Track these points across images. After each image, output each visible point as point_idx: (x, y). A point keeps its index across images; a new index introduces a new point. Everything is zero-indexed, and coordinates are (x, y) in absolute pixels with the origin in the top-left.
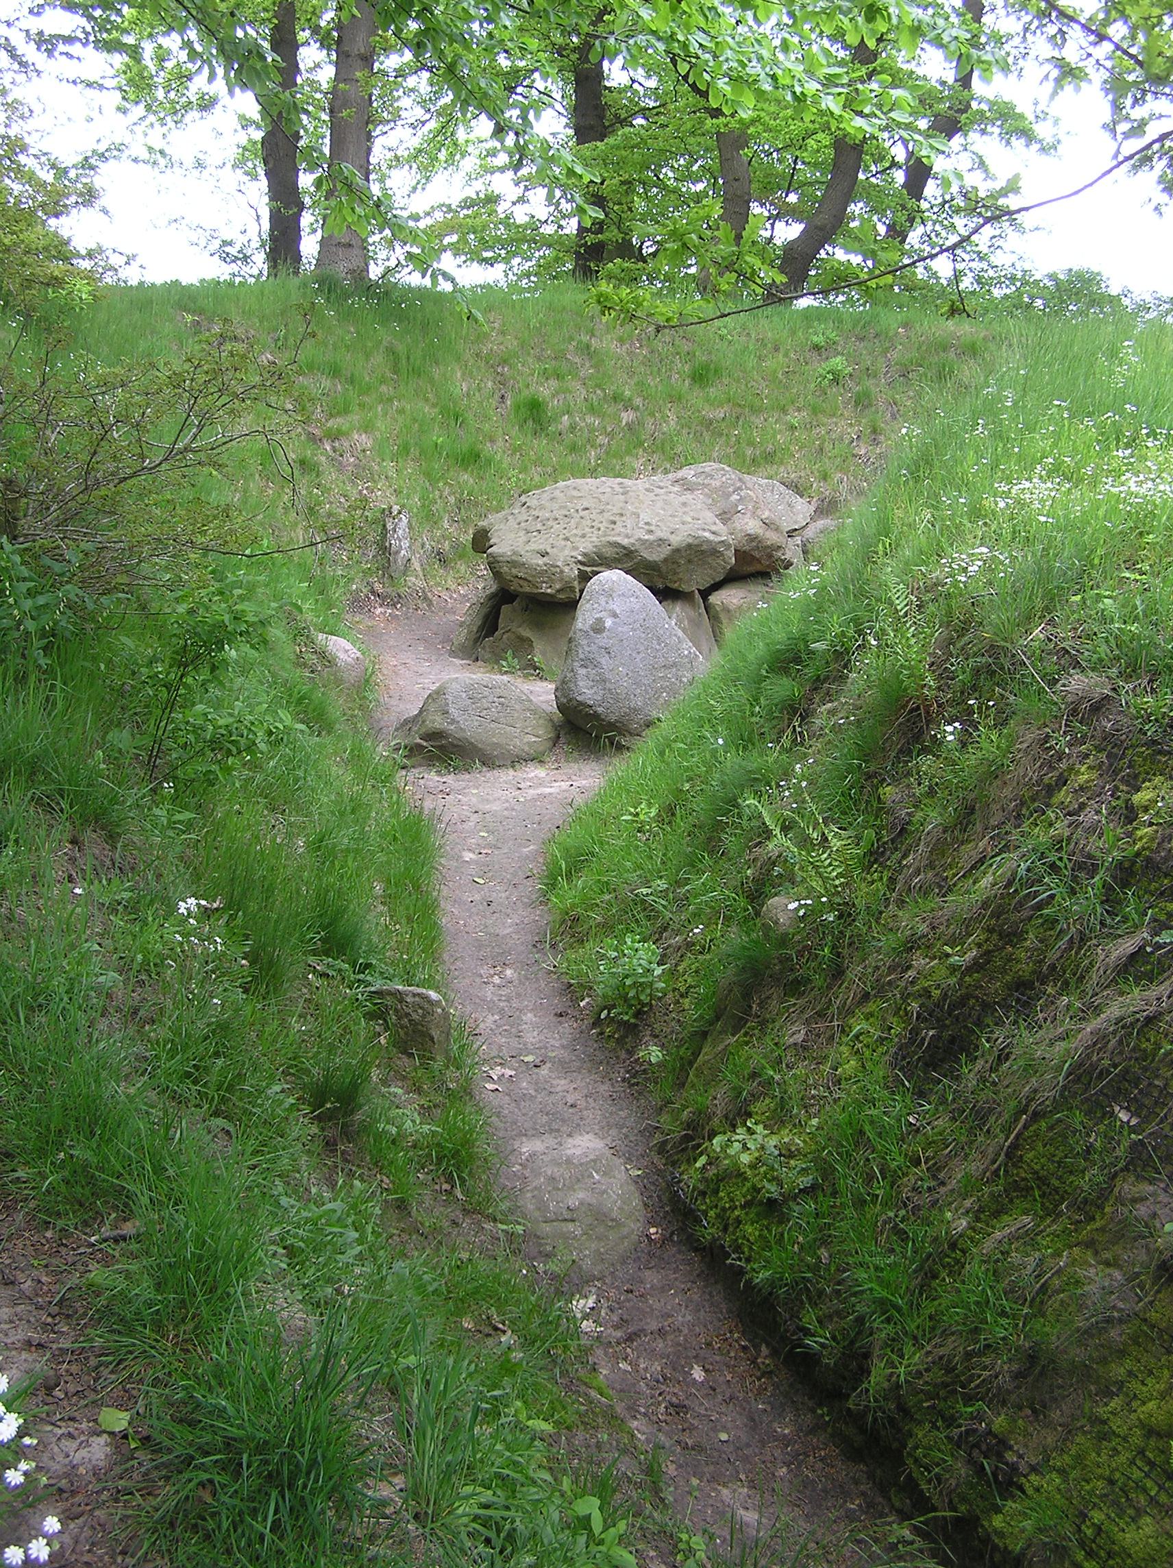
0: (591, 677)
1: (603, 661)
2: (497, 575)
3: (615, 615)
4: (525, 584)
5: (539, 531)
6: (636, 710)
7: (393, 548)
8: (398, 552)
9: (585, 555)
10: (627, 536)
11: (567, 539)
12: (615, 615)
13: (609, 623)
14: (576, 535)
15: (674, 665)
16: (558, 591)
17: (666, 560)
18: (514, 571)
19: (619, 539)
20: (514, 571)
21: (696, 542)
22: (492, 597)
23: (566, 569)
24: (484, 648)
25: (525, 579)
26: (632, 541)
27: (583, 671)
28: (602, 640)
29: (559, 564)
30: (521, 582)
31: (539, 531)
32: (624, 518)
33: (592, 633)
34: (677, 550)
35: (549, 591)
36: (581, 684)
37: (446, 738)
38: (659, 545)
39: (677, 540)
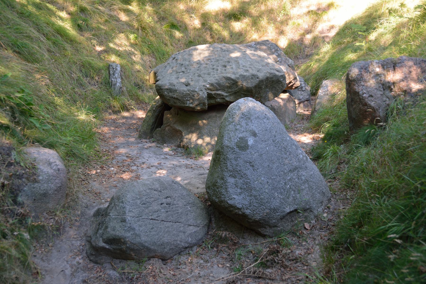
0: (240, 185)
1: (248, 173)
2: (162, 96)
3: (254, 135)
4: (178, 102)
5: (183, 72)
6: (275, 210)
7: (113, 83)
8: (115, 84)
9: (212, 85)
10: (234, 73)
11: (199, 76)
12: (254, 135)
13: (251, 141)
14: (204, 74)
15: (296, 168)
16: (197, 106)
17: (255, 87)
18: (170, 94)
19: (229, 75)
20: (170, 94)
21: (271, 76)
22: (160, 106)
23: (201, 93)
24: (156, 134)
25: (177, 99)
26: (237, 76)
27: (231, 180)
28: (244, 156)
29: (197, 90)
30: (175, 101)
31: (183, 72)
32: (230, 64)
33: (237, 150)
34: (261, 81)
35: (191, 105)
36: (230, 190)
37: (125, 243)
38: (252, 78)
39: (261, 75)
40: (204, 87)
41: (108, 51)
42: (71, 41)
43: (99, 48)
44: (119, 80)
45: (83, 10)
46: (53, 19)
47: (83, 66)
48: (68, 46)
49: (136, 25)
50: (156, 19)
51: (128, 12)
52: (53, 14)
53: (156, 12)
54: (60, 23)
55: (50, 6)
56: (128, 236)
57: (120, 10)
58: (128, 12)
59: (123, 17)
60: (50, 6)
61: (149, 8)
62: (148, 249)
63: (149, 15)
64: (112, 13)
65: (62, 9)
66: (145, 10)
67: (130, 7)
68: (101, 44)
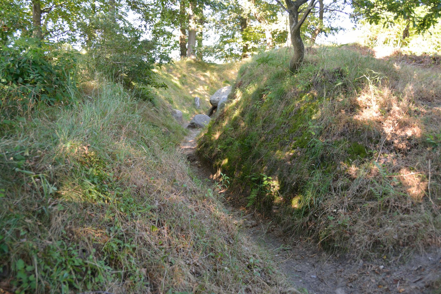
40: (429, 236)
41: (194, 93)
42: (180, 89)
43: (191, 92)
44: (199, 103)
45: (184, 76)
46: (173, 80)
47: (185, 98)
48: (178, 90)
49: (208, 82)
50: (219, 79)
51: (205, 76)
52: (172, 78)
53: (219, 76)
54: (175, 82)
55: (171, 75)
56: (196, 122)
57: (201, 75)
58: (205, 76)
59: (202, 79)
60: (171, 75)
61: (215, 74)
62: (200, 125)
63: (215, 77)
64: (197, 77)
65: (176, 76)
66: (213, 75)
67: (205, 74)
68: (192, 90)
